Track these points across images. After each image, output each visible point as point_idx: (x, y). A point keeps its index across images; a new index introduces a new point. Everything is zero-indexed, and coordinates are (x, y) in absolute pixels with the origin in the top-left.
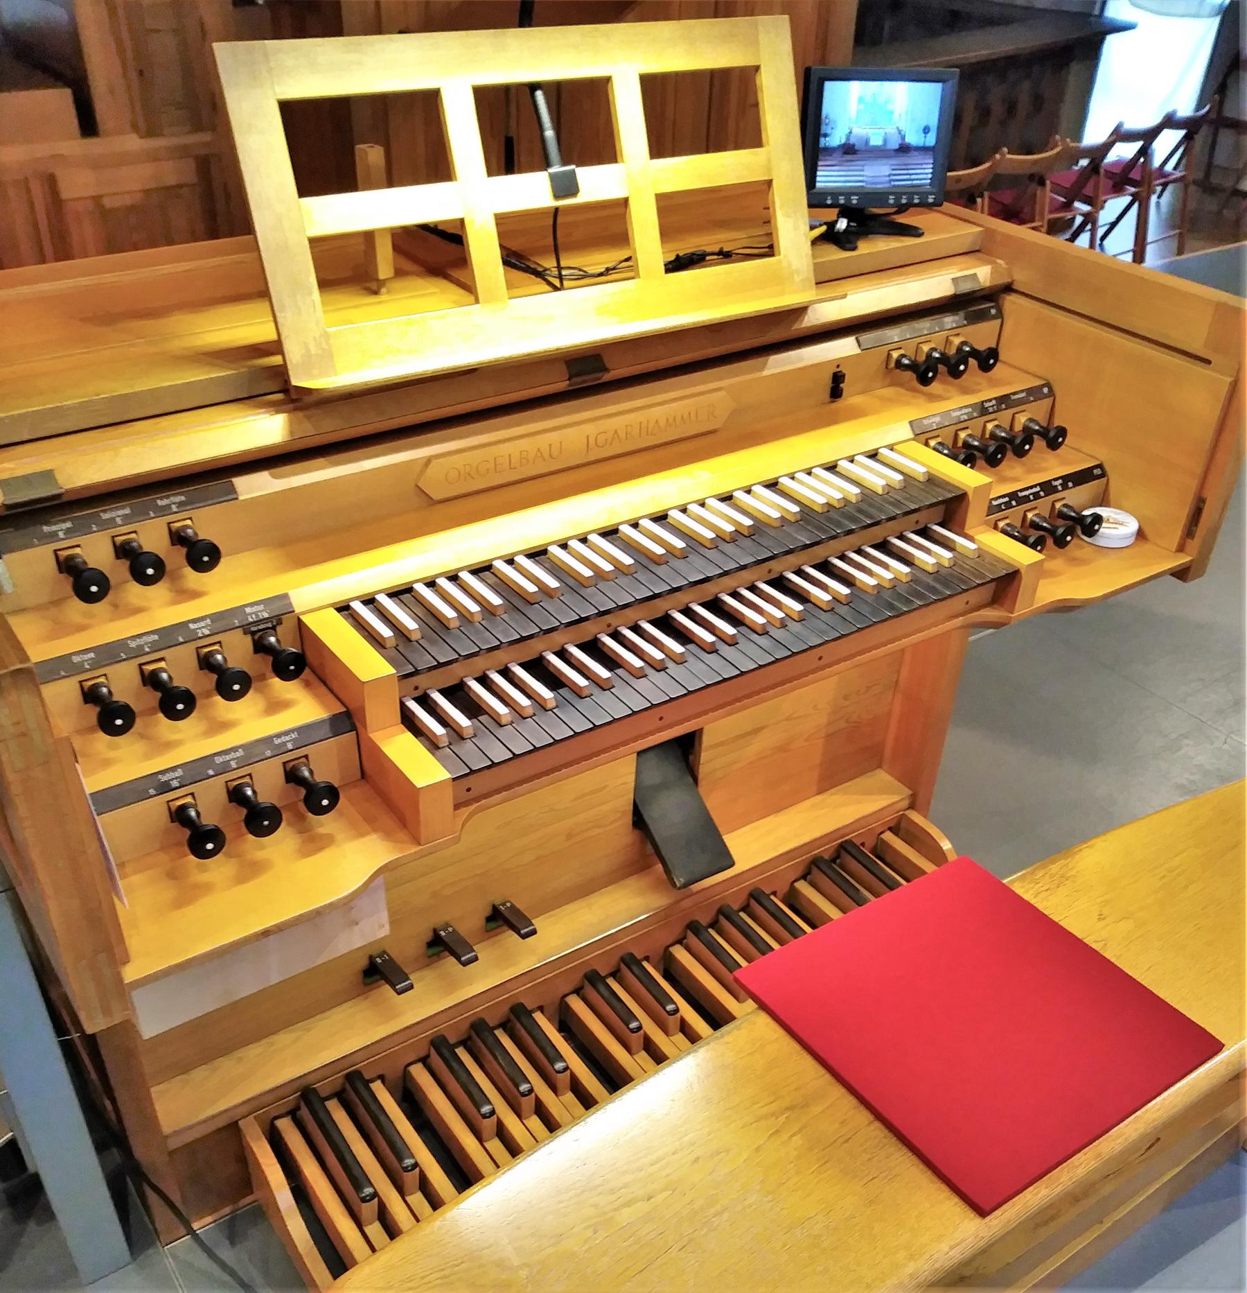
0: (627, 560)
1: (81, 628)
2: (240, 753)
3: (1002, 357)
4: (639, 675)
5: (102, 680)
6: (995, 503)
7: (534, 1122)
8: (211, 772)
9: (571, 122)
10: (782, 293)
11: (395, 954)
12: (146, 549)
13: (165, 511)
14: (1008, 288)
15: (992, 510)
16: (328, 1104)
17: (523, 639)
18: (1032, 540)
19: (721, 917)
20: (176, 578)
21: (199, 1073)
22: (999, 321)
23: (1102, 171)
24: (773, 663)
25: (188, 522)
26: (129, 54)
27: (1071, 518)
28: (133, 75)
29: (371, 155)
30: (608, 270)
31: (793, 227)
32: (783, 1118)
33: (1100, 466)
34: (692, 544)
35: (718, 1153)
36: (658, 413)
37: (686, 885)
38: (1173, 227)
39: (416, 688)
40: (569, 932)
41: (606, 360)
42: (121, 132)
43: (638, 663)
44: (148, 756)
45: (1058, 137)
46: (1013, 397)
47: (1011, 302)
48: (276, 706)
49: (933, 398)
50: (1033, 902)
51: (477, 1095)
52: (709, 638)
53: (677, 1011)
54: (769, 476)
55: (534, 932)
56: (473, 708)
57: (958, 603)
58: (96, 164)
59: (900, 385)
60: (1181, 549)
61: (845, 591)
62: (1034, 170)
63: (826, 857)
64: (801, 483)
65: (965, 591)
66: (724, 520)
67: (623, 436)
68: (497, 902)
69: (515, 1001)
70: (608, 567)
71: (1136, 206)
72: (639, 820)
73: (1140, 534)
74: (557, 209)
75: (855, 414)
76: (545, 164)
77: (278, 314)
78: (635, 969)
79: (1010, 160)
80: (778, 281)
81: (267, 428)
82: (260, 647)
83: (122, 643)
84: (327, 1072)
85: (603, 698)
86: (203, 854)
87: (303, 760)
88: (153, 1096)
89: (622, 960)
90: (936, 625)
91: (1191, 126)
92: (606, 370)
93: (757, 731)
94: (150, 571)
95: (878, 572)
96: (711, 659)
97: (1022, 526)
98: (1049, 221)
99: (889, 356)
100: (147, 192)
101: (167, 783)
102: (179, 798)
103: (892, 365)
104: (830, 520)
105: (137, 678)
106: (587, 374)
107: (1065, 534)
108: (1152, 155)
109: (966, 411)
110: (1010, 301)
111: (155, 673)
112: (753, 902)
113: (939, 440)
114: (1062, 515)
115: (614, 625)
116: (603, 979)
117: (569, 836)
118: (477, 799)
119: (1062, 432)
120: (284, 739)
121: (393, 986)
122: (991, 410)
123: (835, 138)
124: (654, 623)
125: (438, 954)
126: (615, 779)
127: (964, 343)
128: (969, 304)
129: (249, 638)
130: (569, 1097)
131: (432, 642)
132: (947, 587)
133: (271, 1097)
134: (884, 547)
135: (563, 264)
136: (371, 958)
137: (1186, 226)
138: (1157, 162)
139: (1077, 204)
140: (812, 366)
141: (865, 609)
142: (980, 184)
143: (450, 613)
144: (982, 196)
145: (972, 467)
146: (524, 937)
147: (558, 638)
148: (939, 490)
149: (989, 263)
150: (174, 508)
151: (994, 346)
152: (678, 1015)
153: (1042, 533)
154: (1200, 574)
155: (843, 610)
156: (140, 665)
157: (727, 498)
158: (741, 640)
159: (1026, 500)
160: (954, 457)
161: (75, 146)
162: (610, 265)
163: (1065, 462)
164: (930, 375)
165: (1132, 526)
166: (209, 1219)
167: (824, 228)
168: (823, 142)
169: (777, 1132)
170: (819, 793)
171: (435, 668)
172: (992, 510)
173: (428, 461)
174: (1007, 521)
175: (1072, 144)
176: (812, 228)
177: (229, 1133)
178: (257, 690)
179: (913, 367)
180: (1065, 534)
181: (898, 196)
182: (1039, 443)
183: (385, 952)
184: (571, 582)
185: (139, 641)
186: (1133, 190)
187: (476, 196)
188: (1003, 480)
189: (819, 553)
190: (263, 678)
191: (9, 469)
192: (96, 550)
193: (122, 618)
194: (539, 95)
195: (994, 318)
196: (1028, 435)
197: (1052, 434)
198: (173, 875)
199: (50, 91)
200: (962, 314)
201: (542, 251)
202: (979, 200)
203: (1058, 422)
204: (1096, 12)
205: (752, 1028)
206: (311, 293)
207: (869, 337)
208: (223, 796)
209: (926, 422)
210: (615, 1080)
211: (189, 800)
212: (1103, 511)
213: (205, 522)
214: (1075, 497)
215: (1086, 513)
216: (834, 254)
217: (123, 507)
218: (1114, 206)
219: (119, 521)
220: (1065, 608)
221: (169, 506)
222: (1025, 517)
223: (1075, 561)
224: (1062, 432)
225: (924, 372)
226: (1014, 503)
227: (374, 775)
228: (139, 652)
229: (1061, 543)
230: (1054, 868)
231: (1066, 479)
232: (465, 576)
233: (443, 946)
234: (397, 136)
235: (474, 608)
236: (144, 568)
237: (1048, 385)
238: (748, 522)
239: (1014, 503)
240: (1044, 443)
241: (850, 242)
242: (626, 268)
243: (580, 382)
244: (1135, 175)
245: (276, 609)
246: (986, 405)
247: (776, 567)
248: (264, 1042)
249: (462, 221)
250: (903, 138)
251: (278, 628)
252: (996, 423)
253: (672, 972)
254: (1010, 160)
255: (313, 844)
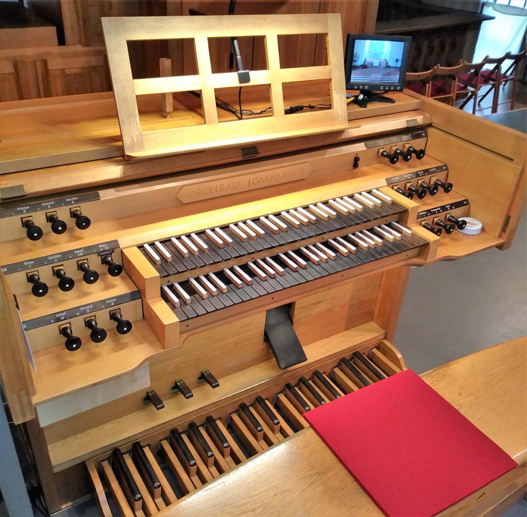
0: (262, 232)
1: (29, 251)
2: (91, 306)
3: (426, 152)
4: (264, 280)
5: (36, 273)
6: (421, 214)
7: (213, 469)
8: (78, 314)
9: (253, 53)
10: (334, 124)
11: (158, 392)
12: (60, 219)
13: (70, 203)
14: (430, 125)
15: (419, 217)
16: (124, 456)
17: (215, 263)
18: (436, 230)
19: (301, 383)
20: (72, 230)
21: (70, 440)
22: (426, 138)
23: (479, 75)
24: (321, 277)
25: (78, 208)
26: (81, 15)
27: (453, 221)
28: (81, 22)
29: (166, 63)
30: (262, 112)
31: (339, 98)
32: (315, 478)
33: (466, 200)
34: (290, 226)
35: (285, 491)
36: (281, 171)
37: (285, 368)
38: (509, 98)
39: (169, 282)
40: (235, 385)
41: (258, 149)
42: (75, 44)
43: (263, 275)
44: (53, 306)
45: (461, 61)
46: (430, 170)
47: (431, 131)
48: (108, 287)
49: (396, 169)
50: (431, 386)
51: (189, 456)
52: (295, 265)
53: (279, 423)
54: (325, 199)
55: (218, 385)
56: (192, 291)
57: (403, 255)
58: (64, 56)
59: (384, 163)
60: (500, 236)
61: (353, 248)
62: (451, 73)
63: (347, 358)
64: (338, 203)
65: (405, 251)
66: (305, 217)
67: (264, 180)
68: (203, 371)
69: (209, 415)
70: (253, 234)
71: (494, 89)
72: (266, 339)
73: (483, 230)
74: (241, 87)
75: (363, 174)
76: (237, 69)
77: (121, 126)
78: (261, 403)
79: (442, 69)
80: (332, 119)
81: (114, 171)
82: (104, 261)
83: (46, 258)
84: (125, 442)
85: (248, 289)
86: (71, 349)
87: (118, 310)
88: (49, 449)
89: (257, 399)
90: (393, 263)
91: (517, 59)
92: (259, 153)
93: (319, 302)
94: (60, 228)
95: (368, 241)
96: (295, 275)
97: (432, 224)
98: (457, 94)
99: (379, 151)
100: (84, 68)
101: (59, 318)
102: (64, 324)
103: (380, 155)
104: (349, 218)
105: (51, 273)
106: (250, 154)
107: (450, 228)
108: (501, 68)
109: (410, 175)
110: (430, 131)
111: (58, 271)
112: (315, 377)
113: (398, 187)
114: (449, 220)
115: (255, 258)
116: (247, 407)
117: (236, 344)
118: (190, 330)
119: (451, 186)
120: (110, 301)
121: (156, 406)
122: (421, 175)
123: (359, 62)
124: (272, 258)
125: (176, 393)
126: (257, 321)
127: (410, 147)
128: (415, 131)
129: (100, 257)
130: (229, 459)
131: (176, 263)
132: (398, 249)
133: (101, 452)
134: (371, 230)
135: (242, 109)
136: (148, 393)
137: (515, 98)
138: (503, 71)
139: (469, 88)
140: (347, 154)
141: (361, 256)
142: (428, 78)
143: (185, 251)
144: (429, 83)
145: (411, 199)
146: (214, 387)
147: (231, 263)
148: (397, 208)
149: (421, 114)
150: (73, 202)
151: (423, 149)
152: (279, 425)
153: (441, 227)
154: (508, 248)
155: (352, 256)
156: (53, 267)
157: (306, 208)
158: (308, 267)
159: (434, 213)
160: (403, 194)
161: (56, 49)
162: (263, 110)
163: (452, 198)
164: (395, 160)
165: (479, 226)
166: (70, 504)
167: (353, 98)
168: (354, 64)
169: (312, 483)
170: (346, 330)
171: (177, 274)
172: (419, 217)
173: (182, 187)
174: (426, 222)
175: (467, 64)
176: (348, 98)
177: (82, 468)
178: (101, 279)
179: (388, 156)
180: (450, 228)
181: (385, 86)
182: (441, 189)
183: (153, 391)
184: (238, 240)
185: (53, 257)
186: (492, 82)
187: (207, 81)
188: (425, 204)
189: (344, 232)
190: (104, 274)
191: (5, 184)
192: (39, 219)
193: (47, 247)
194: (235, 42)
195: (424, 137)
196: (436, 186)
197: (446, 186)
198: (58, 357)
199: (46, 28)
200: (410, 135)
201: (235, 103)
202: (427, 85)
203: (449, 181)
204: (479, 11)
205: (307, 434)
206: (136, 117)
207: (371, 143)
208: (83, 324)
209: (393, 179)
210: (250, 452)
211: (68, 325)
212: (466, 219)
213: (86, 209)
214: (455, 212)
215: (460, 219)
216: (357, 109)
217: (51, 201)
218: (484, 89)
219: (49, 207)
220: (449, 259)
221: (70, 202)
222: (433, 220)
223: (453, 239)
224: (451, 186)
225: (392, 158)
226: (429, 214)
227: (149, 318)
228: (53, 261)
229: (448, 232)
230: (441, 371)
231: (452, 205)
232: (194, 235)
233: (180, 389)
234: (178, 56)
235: (195, 249)
236: (58, 226)
237: (446, 165)
238: (314, 218)
239: (429, 214)
240: (443, 189)
241: (364, 104)
242: (268, 112)
243: (247, 157)
244: (493, 77)
245: (112, 246)
246: (419, 173)
247: (326, 237)
248: (99, 427)
249: (201, 91)
250: (387, 63)
251: (112, 254)
252: (423, 180)
253: (278, 406)
254: (442, 69)
255: (119, 347)
